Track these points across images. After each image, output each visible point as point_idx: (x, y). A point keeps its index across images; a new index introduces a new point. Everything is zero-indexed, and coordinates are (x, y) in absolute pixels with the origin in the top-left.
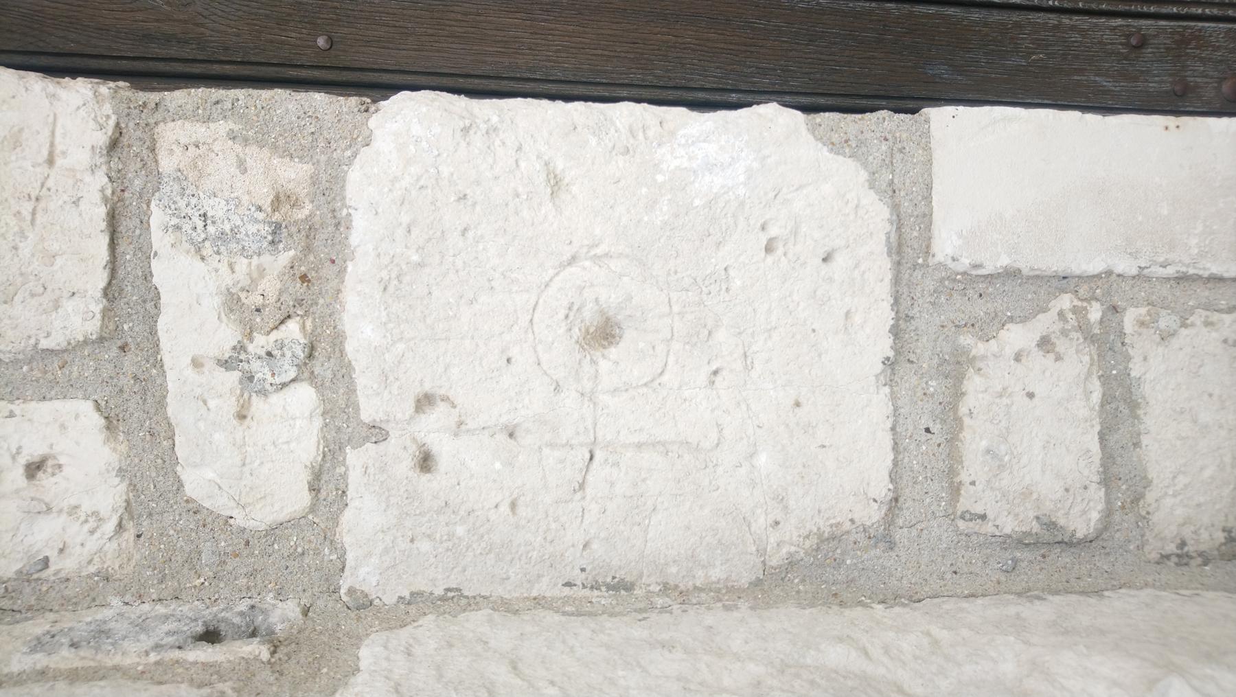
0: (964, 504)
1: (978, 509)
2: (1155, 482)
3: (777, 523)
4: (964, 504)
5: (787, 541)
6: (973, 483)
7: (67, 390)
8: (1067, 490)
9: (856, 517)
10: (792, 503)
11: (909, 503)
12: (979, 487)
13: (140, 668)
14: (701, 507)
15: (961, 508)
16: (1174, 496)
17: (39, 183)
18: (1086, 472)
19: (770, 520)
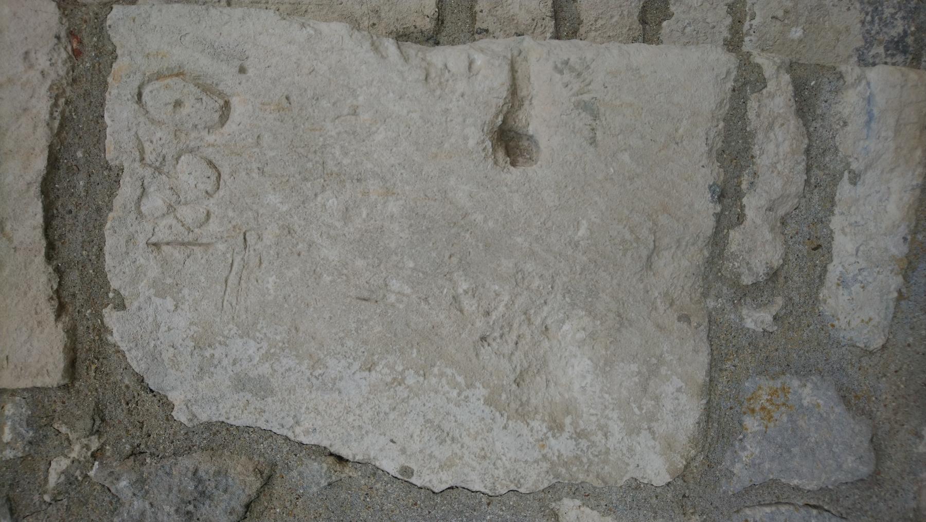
0: (478, 25)
1: (484, 26)
2: (585, 21)
3: (374, 24)
4: (478, 25)
5: (523, 93)
6: (481, 11)
7: (100, 27)
8: (533, 20)
9: (418, 24)
10: (383, 15)
11: (449, 24)
12: (485, 14)
13: (836, 323)
14: (333, 13)
15: (476, 26)
16: (596, 30)
17: (447, 23)
18: (544, 10)
19: (371, 22)
